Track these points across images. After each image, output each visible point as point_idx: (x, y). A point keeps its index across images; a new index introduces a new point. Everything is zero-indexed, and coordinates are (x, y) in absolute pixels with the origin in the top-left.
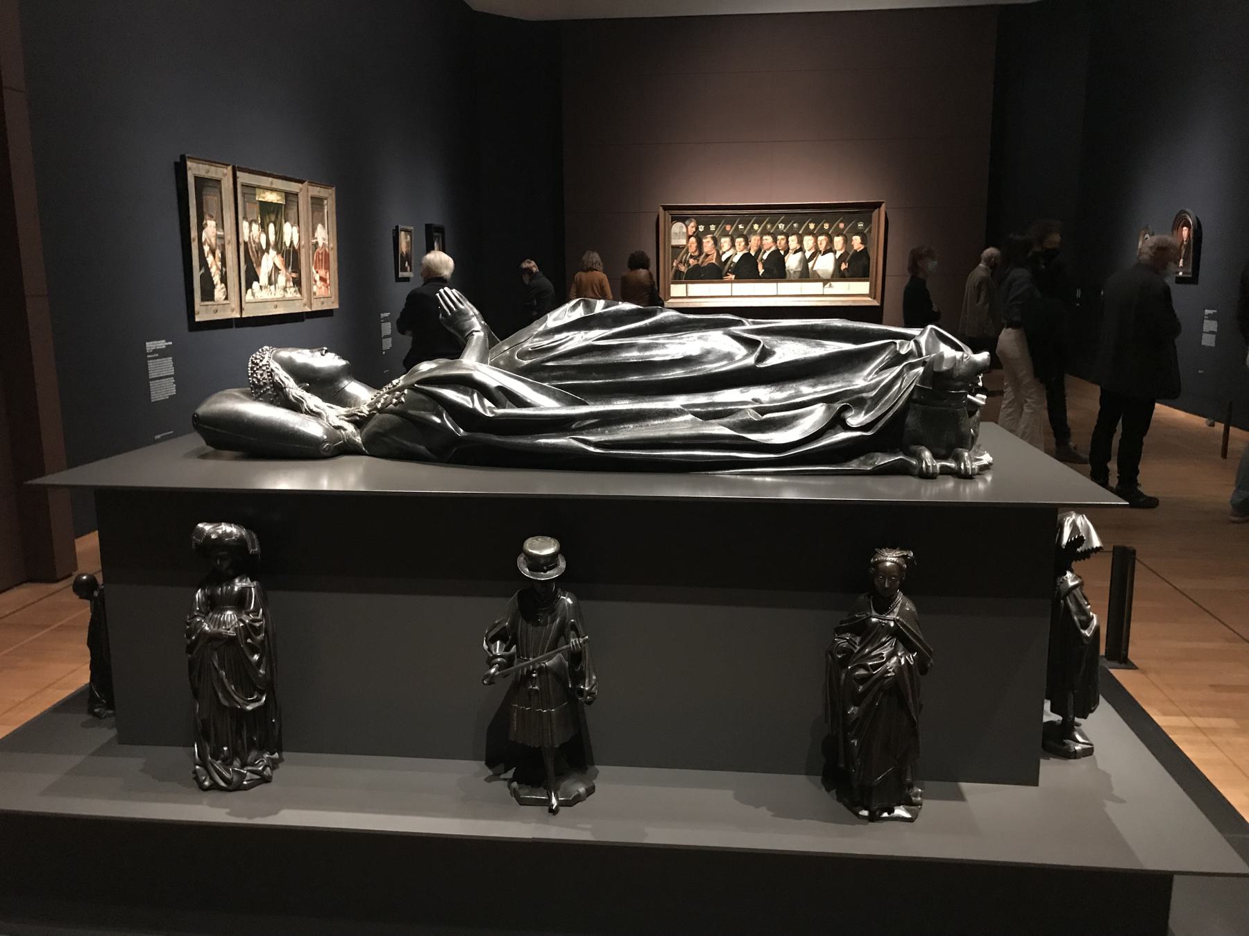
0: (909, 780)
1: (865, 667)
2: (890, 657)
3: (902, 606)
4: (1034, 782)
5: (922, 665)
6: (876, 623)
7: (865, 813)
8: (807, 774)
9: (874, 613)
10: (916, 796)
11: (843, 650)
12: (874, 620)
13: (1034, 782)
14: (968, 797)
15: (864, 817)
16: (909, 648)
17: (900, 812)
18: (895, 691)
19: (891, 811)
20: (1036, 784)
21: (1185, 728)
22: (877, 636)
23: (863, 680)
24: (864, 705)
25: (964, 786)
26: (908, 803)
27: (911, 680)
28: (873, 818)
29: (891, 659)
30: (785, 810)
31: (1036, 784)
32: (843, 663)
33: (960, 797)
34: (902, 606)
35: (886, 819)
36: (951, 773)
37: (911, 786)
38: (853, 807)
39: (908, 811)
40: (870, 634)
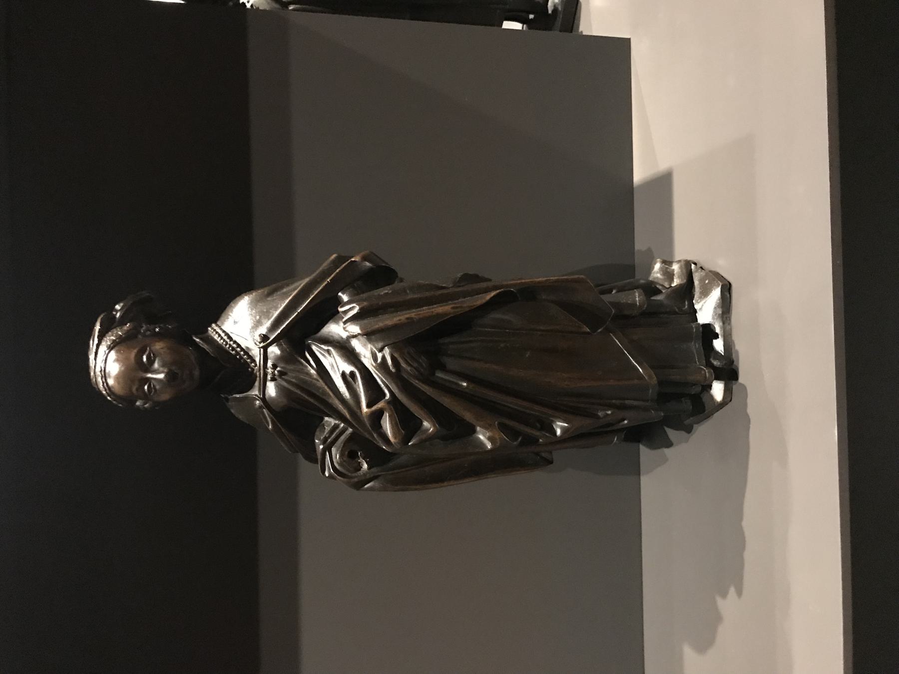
0: (637, 297)
1: (377, 416)
2: (351, 356)
3: (243, 325)
4: (622, 47)
5: (372, 280)
6: (279, 388)
7: (718, 390)
8: (638, 474)
9: (255, 392)
10: (670, 276)
11: (350, 455)
12: (271, 390)
13: (622, 47)
14: (662, 166)
15: (728, 391)
16: (327, 310)
17: (706, 310)
18: (423, 346)
19: (708, 332)
20: (629, 39)
21: (666, 313)
22: (305, 386)
23: (407, 424)
24: (468, 416)
25: (640, 174)
26: (687, 291)
27: (396, 307)
28: (728, 372)
29: (351, 353)
30: (725, 562)
31: (629, 39)
32: (379, 458)
33: (663, 184)
34: (243, 325)
35: (728, 345)
36: (616, 202)
37: (651, 289)
38: (700, 407)
39: (705, 293)
40: (306, 407)
